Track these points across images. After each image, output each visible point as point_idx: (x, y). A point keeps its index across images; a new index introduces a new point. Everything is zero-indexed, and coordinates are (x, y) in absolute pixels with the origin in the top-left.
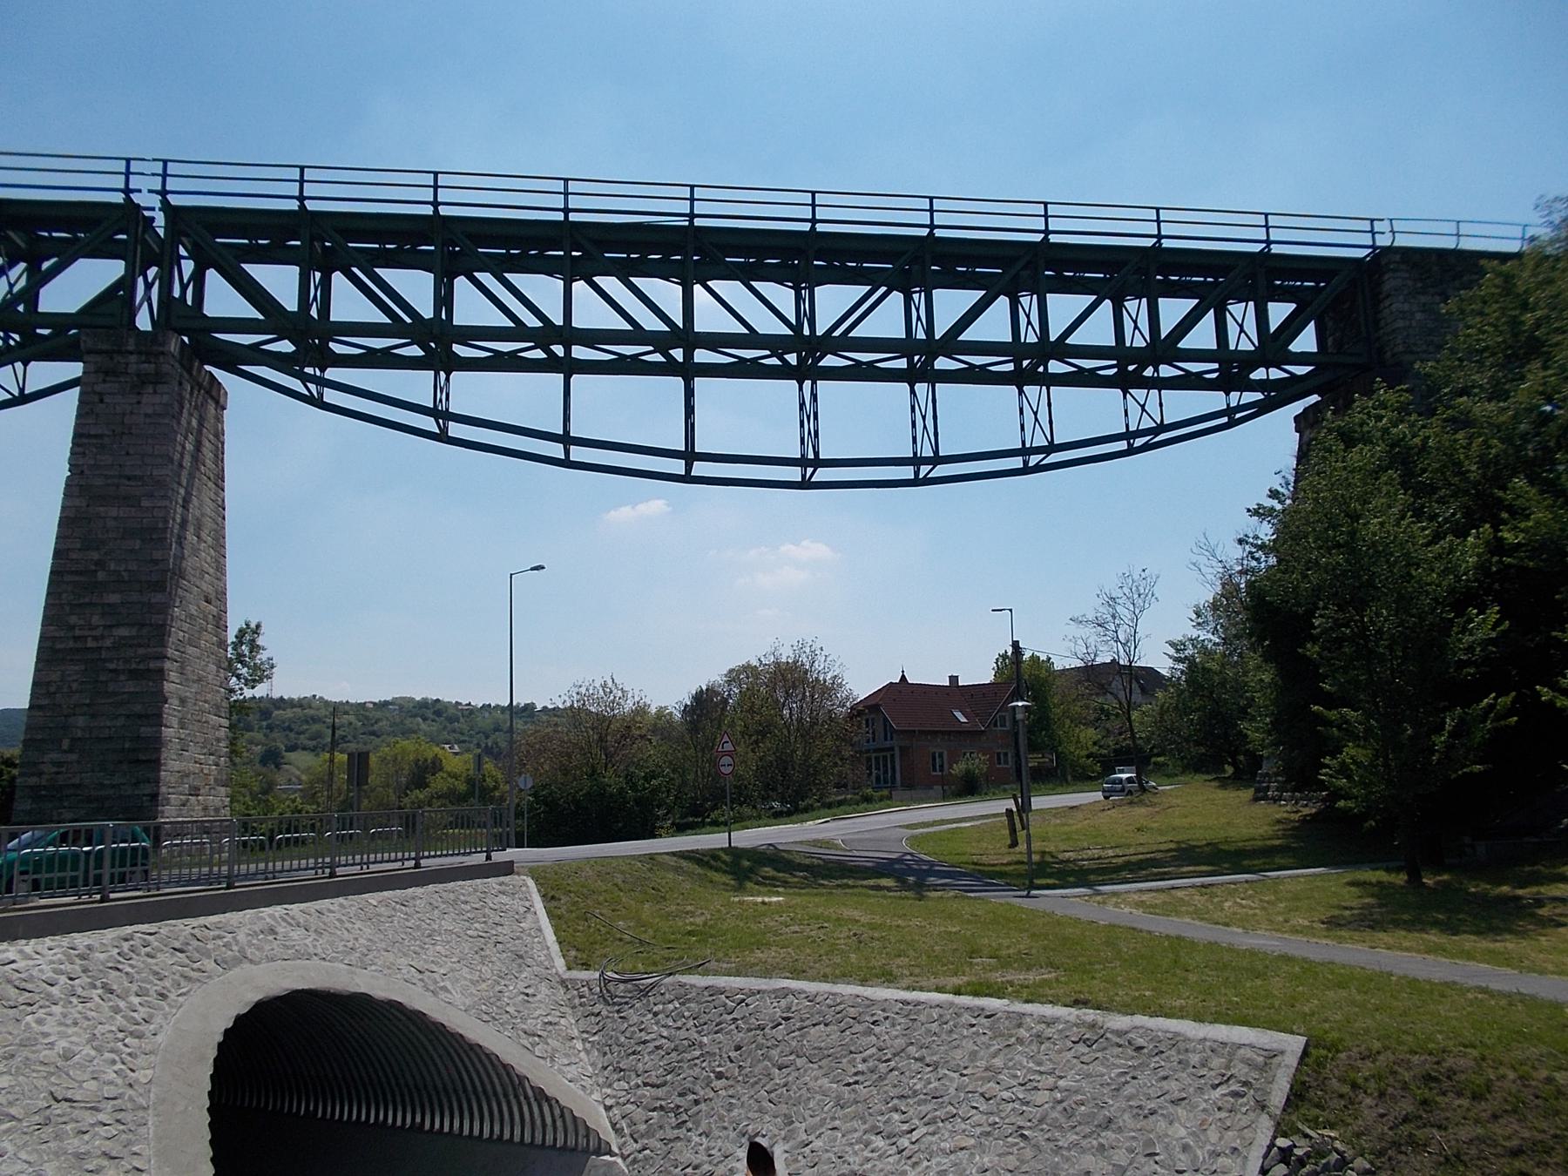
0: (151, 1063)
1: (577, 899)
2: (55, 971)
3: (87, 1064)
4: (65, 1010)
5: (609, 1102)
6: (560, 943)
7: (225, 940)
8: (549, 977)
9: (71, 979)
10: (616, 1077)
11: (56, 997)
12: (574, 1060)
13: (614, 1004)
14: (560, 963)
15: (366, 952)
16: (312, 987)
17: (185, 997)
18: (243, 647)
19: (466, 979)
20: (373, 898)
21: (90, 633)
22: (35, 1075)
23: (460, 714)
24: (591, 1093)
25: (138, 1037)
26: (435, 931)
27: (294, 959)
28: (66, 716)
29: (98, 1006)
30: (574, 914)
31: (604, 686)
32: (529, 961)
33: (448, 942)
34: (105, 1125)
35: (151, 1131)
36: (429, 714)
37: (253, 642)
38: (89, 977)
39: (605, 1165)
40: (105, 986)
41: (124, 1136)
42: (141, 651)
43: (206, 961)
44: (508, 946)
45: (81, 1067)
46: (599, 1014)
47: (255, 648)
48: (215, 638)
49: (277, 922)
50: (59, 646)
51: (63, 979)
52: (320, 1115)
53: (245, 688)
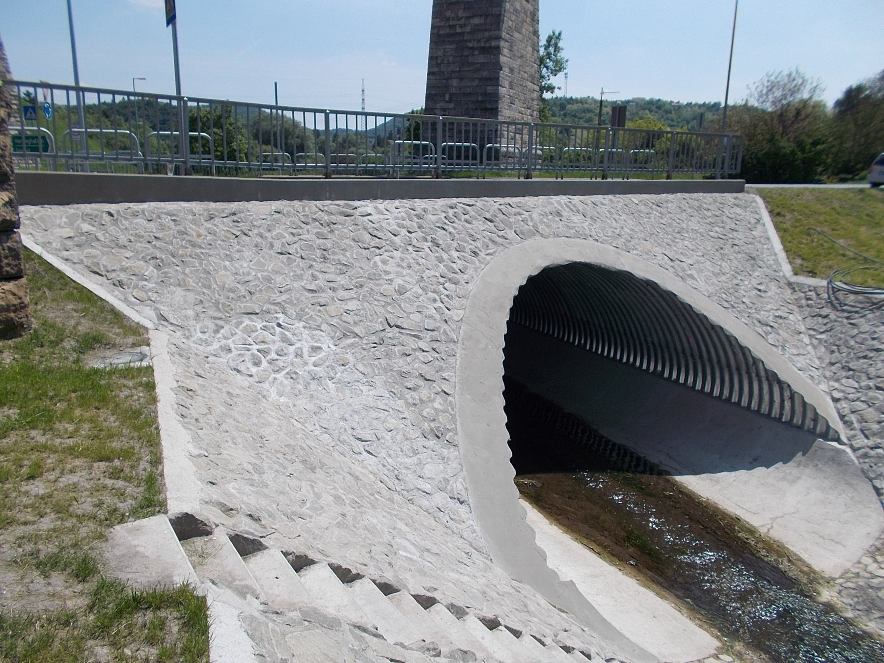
0: (462, 306)
1: (800, 217)
2: (399, 225)
3: (415, 299)
4: (403, 256)
5: (837, 395)
6: (787, 251)
7: (523, 216)
8: (778, 278)
9: (409, 232)
10: (844, 374)
11: (397, 245)
12: (802, 351)
13: (843, 311)
14: (786, 269)
15: (630, 239)
16: (587, 261)
17: (492, 257)
18: (551, 48)
19: (709, 271)
20: (635, 198)
21: (458, 22)
22: (376, 303)
23: (672, 108)
24: (819, 383)
25: (455, 283)
26: (683, 229)
27: (574, 238)
28: (446, 79)
29: (427, 255)
30: (798, 229)
31: (790, 75)
32: (761, 263)
33: (694, 239)
34: (424, 351)
35: (458, 362)
36: (654, 108)
37: (556, 45)
38: (422, 232)
39: (833, 450)
40: (433, 241)
41: (437, 363)
42: (487, 34)
43: (508, 231)
44: (743, 248)
45: (410, 301)
46: (826, 317)
47: (557, 49)
48: (531, 29)
49: (562, 207)
50: (442, 32)
51: (404, 232)
52: (588, 348)
53: (551, 75)
